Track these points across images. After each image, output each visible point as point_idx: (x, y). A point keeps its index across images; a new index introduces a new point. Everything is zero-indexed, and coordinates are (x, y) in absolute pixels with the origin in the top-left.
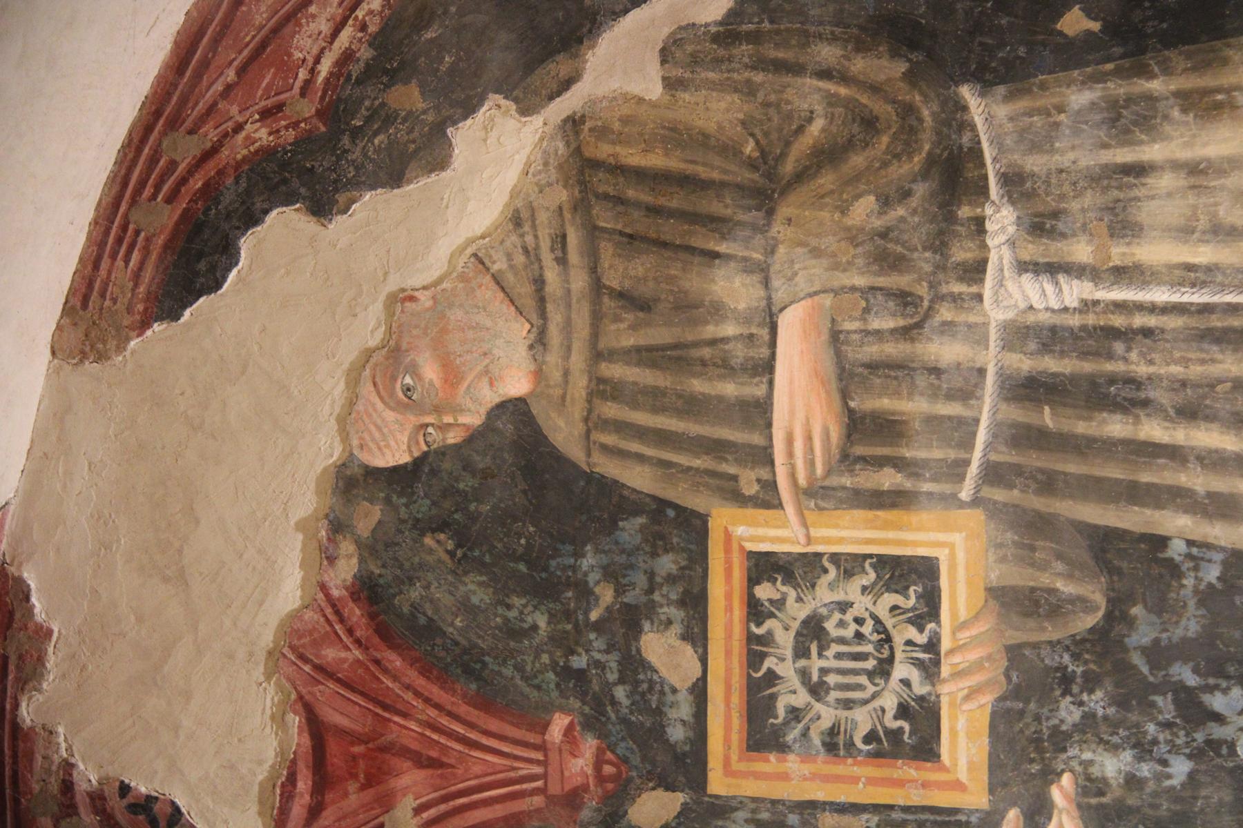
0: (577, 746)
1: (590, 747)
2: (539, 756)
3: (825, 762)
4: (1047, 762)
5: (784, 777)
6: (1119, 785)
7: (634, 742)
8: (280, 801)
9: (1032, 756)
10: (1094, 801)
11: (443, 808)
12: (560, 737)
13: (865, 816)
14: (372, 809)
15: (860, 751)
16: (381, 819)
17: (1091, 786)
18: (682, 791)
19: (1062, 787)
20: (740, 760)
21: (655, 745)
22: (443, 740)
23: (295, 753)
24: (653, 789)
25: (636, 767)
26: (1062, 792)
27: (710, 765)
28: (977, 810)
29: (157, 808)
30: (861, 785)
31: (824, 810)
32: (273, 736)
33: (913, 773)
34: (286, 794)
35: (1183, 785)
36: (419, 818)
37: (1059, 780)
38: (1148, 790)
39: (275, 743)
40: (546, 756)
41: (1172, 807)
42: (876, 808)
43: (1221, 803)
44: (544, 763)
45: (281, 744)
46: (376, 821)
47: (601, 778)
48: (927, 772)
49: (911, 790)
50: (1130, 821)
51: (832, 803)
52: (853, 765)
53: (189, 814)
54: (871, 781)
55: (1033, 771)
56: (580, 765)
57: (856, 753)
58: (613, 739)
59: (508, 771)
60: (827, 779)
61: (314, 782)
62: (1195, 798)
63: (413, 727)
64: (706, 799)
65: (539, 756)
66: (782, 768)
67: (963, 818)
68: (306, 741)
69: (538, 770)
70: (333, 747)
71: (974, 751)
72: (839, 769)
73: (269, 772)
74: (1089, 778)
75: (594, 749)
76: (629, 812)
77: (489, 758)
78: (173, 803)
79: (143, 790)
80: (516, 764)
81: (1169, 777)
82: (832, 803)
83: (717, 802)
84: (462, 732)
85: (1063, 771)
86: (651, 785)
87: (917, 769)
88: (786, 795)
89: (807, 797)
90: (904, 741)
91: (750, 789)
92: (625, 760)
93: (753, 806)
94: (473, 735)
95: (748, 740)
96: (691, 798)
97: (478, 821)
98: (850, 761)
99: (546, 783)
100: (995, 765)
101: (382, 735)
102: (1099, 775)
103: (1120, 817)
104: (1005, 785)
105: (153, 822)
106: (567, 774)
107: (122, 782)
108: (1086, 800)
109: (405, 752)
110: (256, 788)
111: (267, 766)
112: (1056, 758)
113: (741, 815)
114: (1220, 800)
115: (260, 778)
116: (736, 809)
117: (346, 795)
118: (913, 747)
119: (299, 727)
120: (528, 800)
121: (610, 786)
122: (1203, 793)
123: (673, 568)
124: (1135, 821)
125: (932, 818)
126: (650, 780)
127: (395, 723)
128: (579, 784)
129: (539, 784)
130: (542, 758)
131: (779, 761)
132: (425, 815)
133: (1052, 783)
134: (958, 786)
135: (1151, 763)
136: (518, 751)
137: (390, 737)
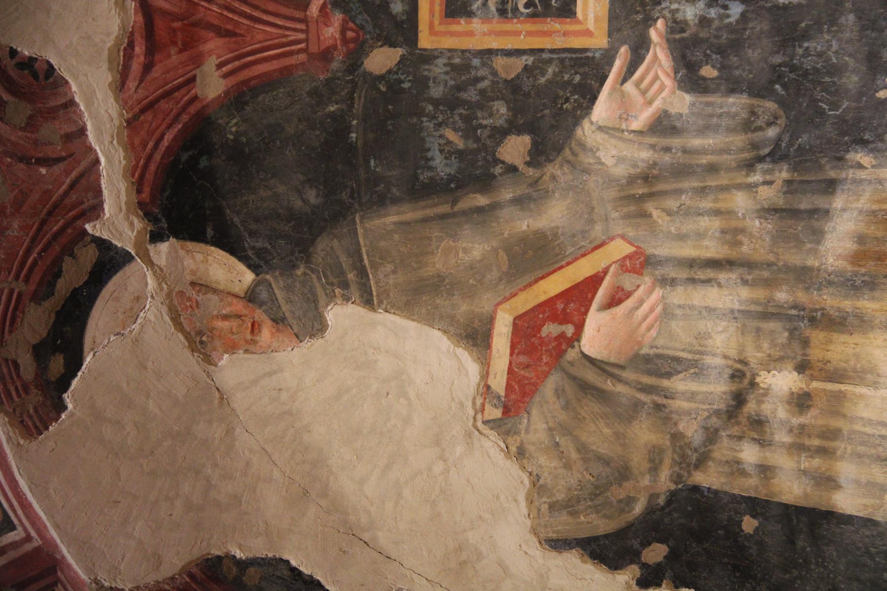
0: (329, 19)
1: (338, 19)
2: (303, 27)
3: (497, 23)
4: (647, 12)
5: (470, 34)
6: (695, 25)
7: (369, 15)
8: (124, 60)
9: (638, 9)
10: (678, 36)
11: (237, 63)
12: (317, 13)
13: (525, 58)
14: (188, 65)
15: (522, 13)
16: (194, 72)
17: (677, 26)
18: (400, 47)
19: (657, 28)
20: (441, 24)
21: (382, 16)
22: (236, 18)
23: (133, 27)
24: (381, 46)
25: (370, 32)
26: (656, 33)
27: (420, 28)
28: (600, 49)
29: (37, 65)
30: (522, 37)
31: (497, 55)
32: (117, 16)
33: (558, 26)
34: (127, 56)
35: (737, 22)
36: (220, 71)
37: (655, 24)
38: (714, 27)
39: (118, 21)
40: (307, 26)
41: (730, 36)
42: (532, 52)
43: (762, 32)
44: (306, 31)
45: (122, 21)
46: (191, 74)
47: (345, 40)
48: (569, 26)
49: (556, 38)
50: (701, 48)
51: (502, 49)
52: (517, 23)
53: (60, 69)
54: (529, 34)
55: (638, 19)
56: (331, 32)
57: (519, 15)
58: (353, 13)
59: (282, 37)
60: (499, 34)
61: (147, 47)
62: (745, 29)
63: (215, 9)
64: (417, 51)
65: (303, 27)
66: (468, 28)
67: (590, 54)
68: (140, 18)
69: (301, 36)
70: (159, 23)
71: (598, 9)
72: (508, 27)
73: (115, 41)
74: (675, 21)
75: (341, 21)
76: (365, 62)
77: (268, 29)
78: (48, 62)
79: (26, 53)
80: (287, 33)
81: (728, 16)
82: (502, 50)
83: (424, 53)
84: (249, 11)
85: (658, 18)
86: (379, 44)
87: (560, 23)
88: (471, 46)
89: (486, 47)
90: (552, 5)
91: (448, 43)
92: (362, 28)
93: (449, 54)
94: (256, 14)
95: (446, 9)
96: (407, 52)
97: (260, 72)
98: (515, 21)
99: (307, 46)
100: (613, 17)
101: (193, 15)
102: (682, 18)
103: (695, 46)
104: (619, 30)
105: (35, 75)
106: (322, 38)
107: (11, 48)
108: (673, 36)
109: (210, 26)
110: (106, 52)
111: (113, 37)
112: (654, 9)
113: (441, 61)
114: (761, 29)
115: (109, 45)
116: (438, 57)
117: (169, 56)
118: (558, 9)
119: (134, 9)
120: (295, 57)
121: (352, 46)
122: (751, 25)
123: (500, 171)
124: (705, 48)
125: (569, 56)
126: (379, 41)
127: (202, 6)
128: (330, 45)
129: (303, 45)
130: (304, 28)
131: (467, 23)
132: (224, 69)
133: (650, 26)
134: (588, 33)
135: (717, 8)
136: (289, 24)
137: (198, 17)
